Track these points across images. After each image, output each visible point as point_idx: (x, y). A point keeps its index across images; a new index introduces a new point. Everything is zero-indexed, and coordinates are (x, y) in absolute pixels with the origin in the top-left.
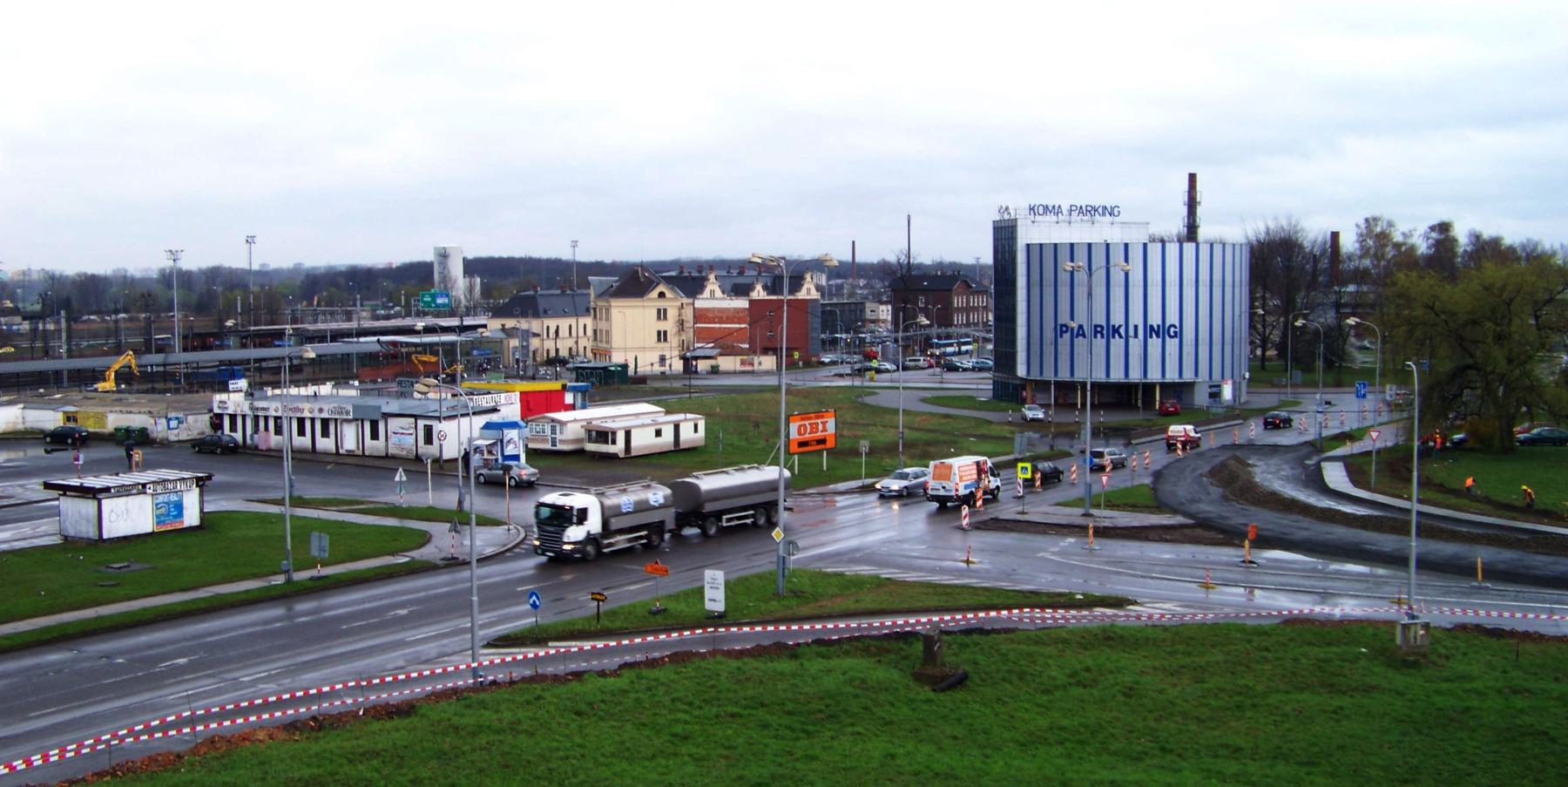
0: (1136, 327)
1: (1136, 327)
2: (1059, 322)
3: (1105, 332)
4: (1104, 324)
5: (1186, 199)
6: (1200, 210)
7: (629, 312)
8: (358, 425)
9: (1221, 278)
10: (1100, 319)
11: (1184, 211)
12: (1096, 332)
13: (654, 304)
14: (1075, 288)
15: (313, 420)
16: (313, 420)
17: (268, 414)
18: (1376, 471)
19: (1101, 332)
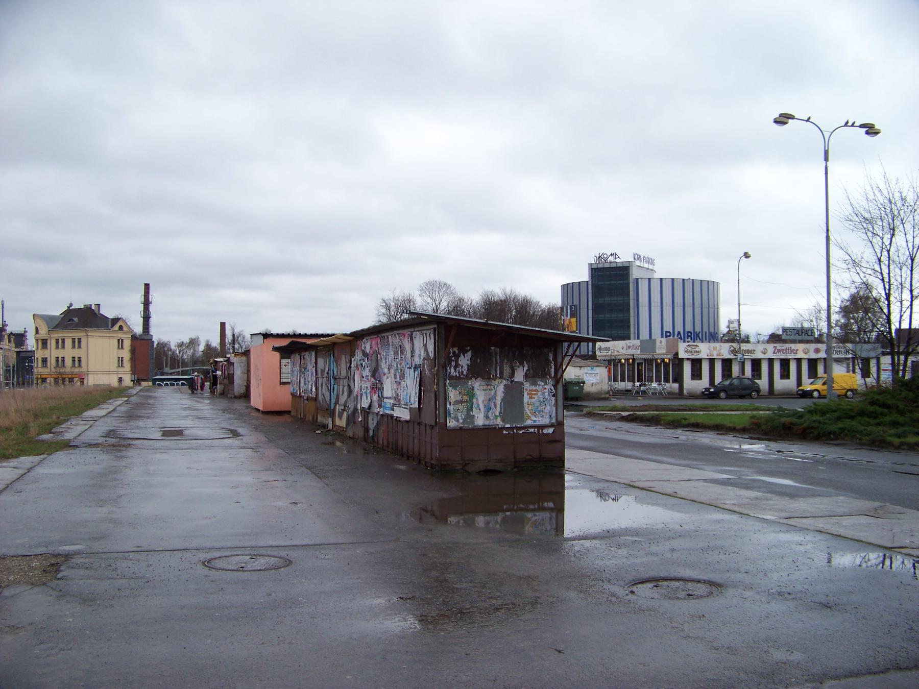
0: (706, 333)
1: (706, 333)
2: (664, 331)
3: (692, 336)
4: (671, 331)
5: (143, 300)
6: (151, 308)
7: (100, 340)
8: (848, 365)
9: (700, 303)
10: (689, 328)
11: (142, 307)
12: (688, 336)
13: (116, 335)
14: (640, 308)
15: (712, 361)
16: (712, 361)
17: (798, 356)
18: (204, 369)
19: (690, 336)
